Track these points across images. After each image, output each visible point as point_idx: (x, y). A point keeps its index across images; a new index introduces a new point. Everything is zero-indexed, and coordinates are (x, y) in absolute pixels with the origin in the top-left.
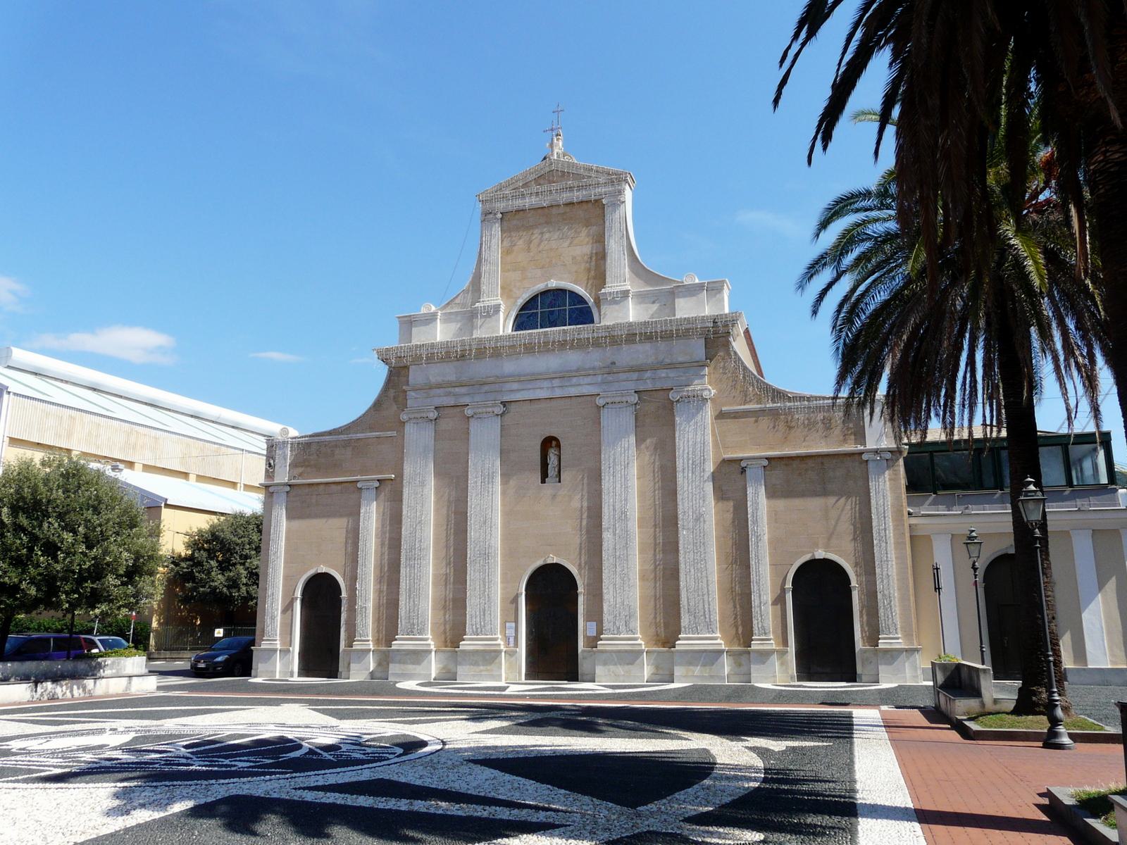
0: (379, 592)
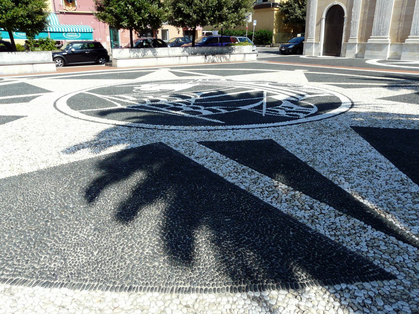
0: (364, 13)
